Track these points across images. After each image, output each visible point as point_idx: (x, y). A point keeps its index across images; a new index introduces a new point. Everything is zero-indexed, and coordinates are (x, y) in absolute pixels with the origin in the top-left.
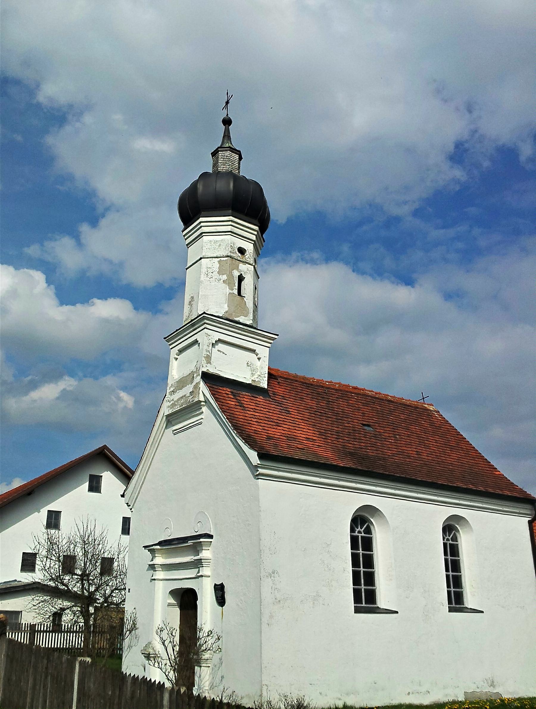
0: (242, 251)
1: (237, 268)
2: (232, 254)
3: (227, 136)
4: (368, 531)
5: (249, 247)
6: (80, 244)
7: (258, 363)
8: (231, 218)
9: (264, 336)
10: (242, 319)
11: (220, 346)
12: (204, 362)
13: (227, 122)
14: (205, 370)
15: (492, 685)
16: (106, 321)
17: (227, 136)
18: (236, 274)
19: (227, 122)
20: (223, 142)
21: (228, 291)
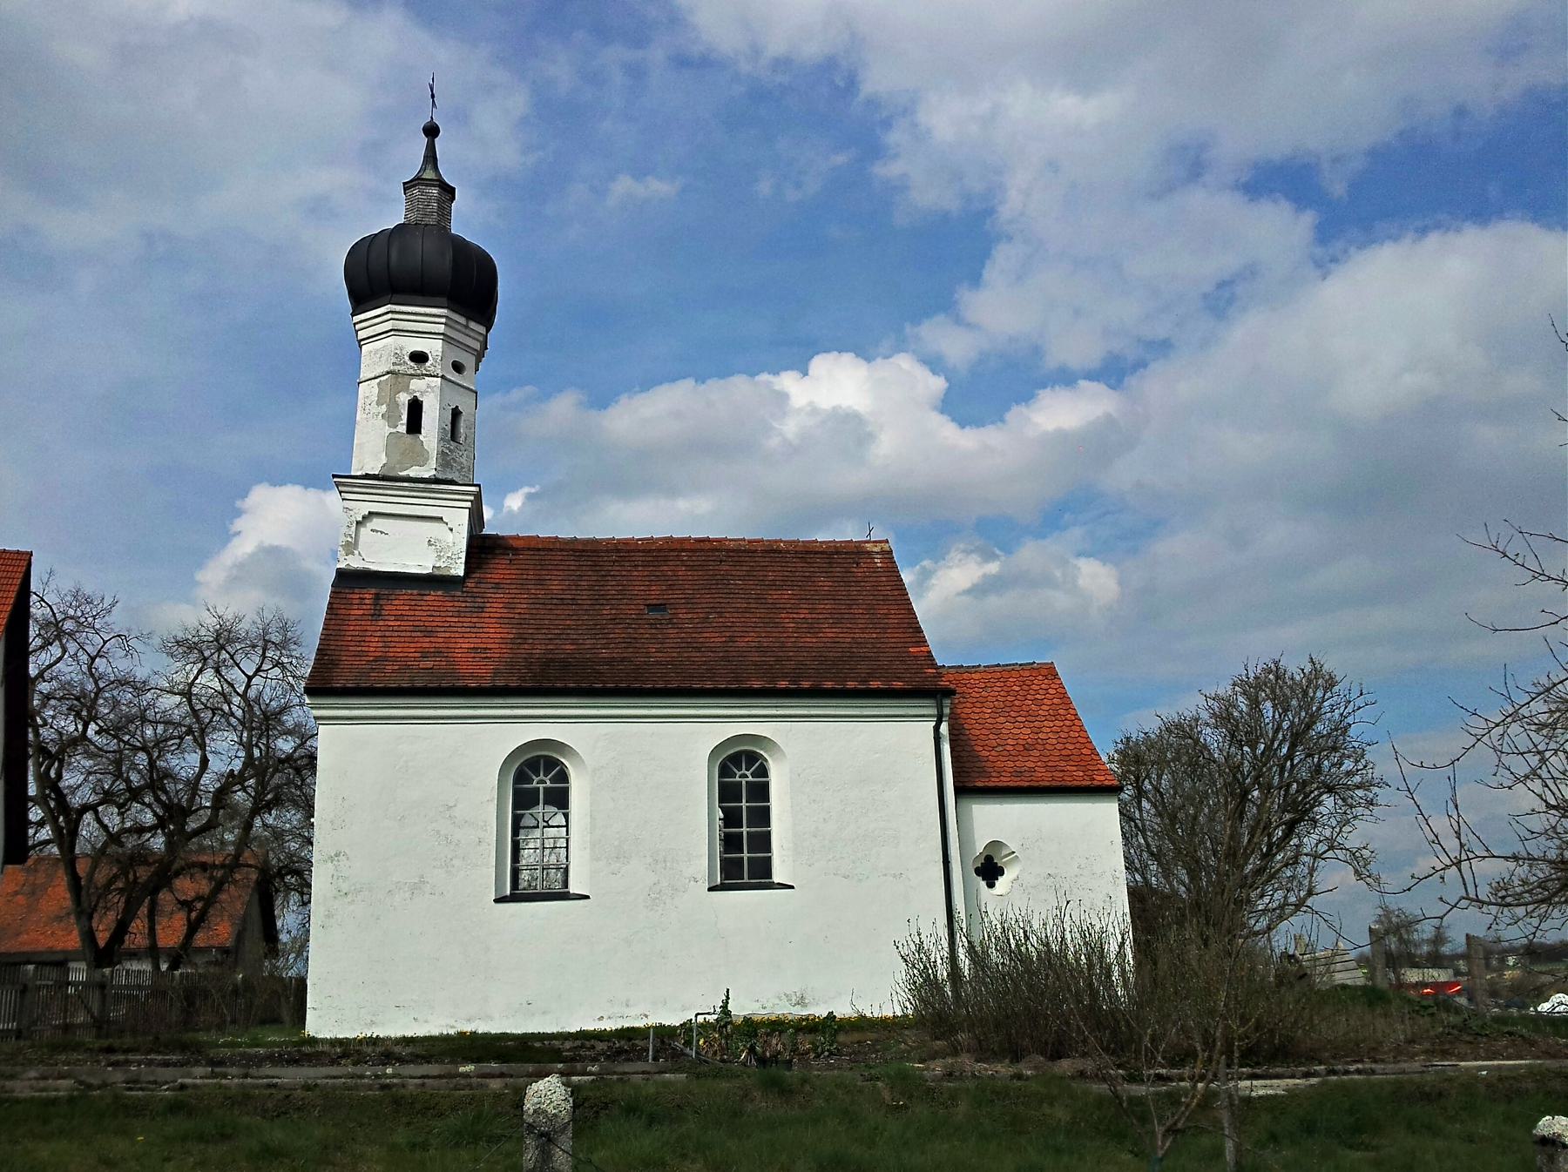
0: (419, 358)
1: (406, 389)
2: (397, 368)
3: (431, 158)
4: (763, 771)
5: (433, 347)
6: (959, 321)
7: (450, 537)
8: (389, 307)
9: (453, 492)
10: (413, 472)
11: (376, 523)
12: (341, 553)
13: (431, 131)
14: (342, 565)
15: (801, 1002)
16: (1062, 436)
17: (431, 158)
18: (404, 398)
19: (431, 131)
20: (423, 169)
21: (388, 430)
